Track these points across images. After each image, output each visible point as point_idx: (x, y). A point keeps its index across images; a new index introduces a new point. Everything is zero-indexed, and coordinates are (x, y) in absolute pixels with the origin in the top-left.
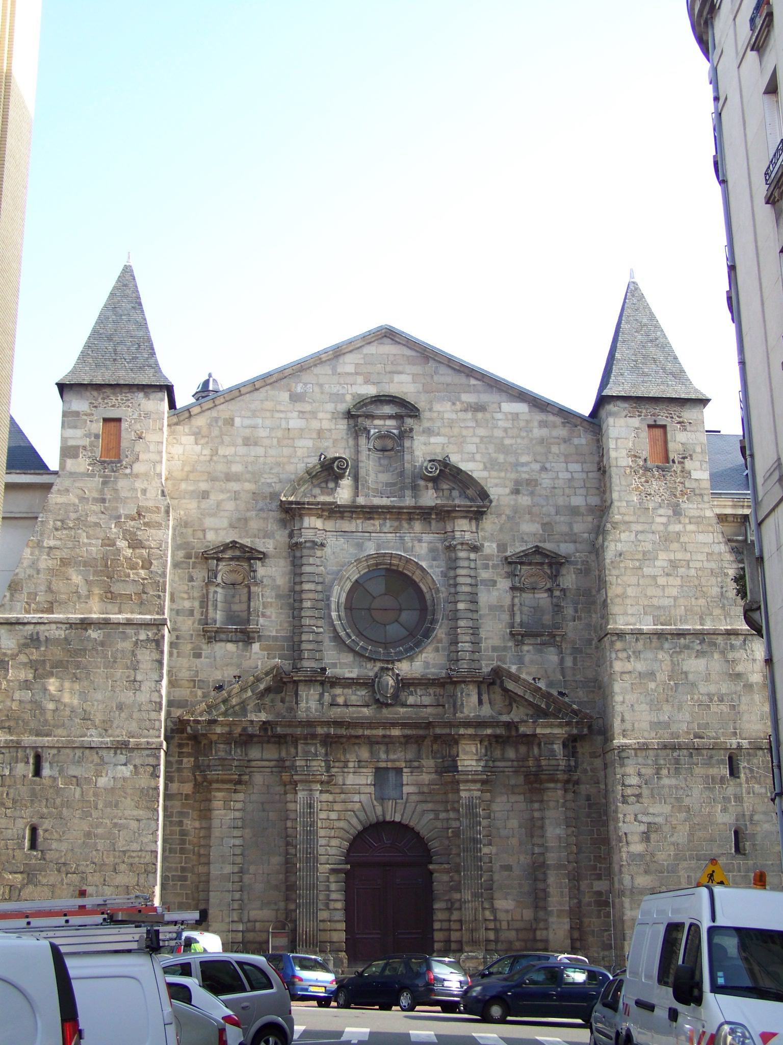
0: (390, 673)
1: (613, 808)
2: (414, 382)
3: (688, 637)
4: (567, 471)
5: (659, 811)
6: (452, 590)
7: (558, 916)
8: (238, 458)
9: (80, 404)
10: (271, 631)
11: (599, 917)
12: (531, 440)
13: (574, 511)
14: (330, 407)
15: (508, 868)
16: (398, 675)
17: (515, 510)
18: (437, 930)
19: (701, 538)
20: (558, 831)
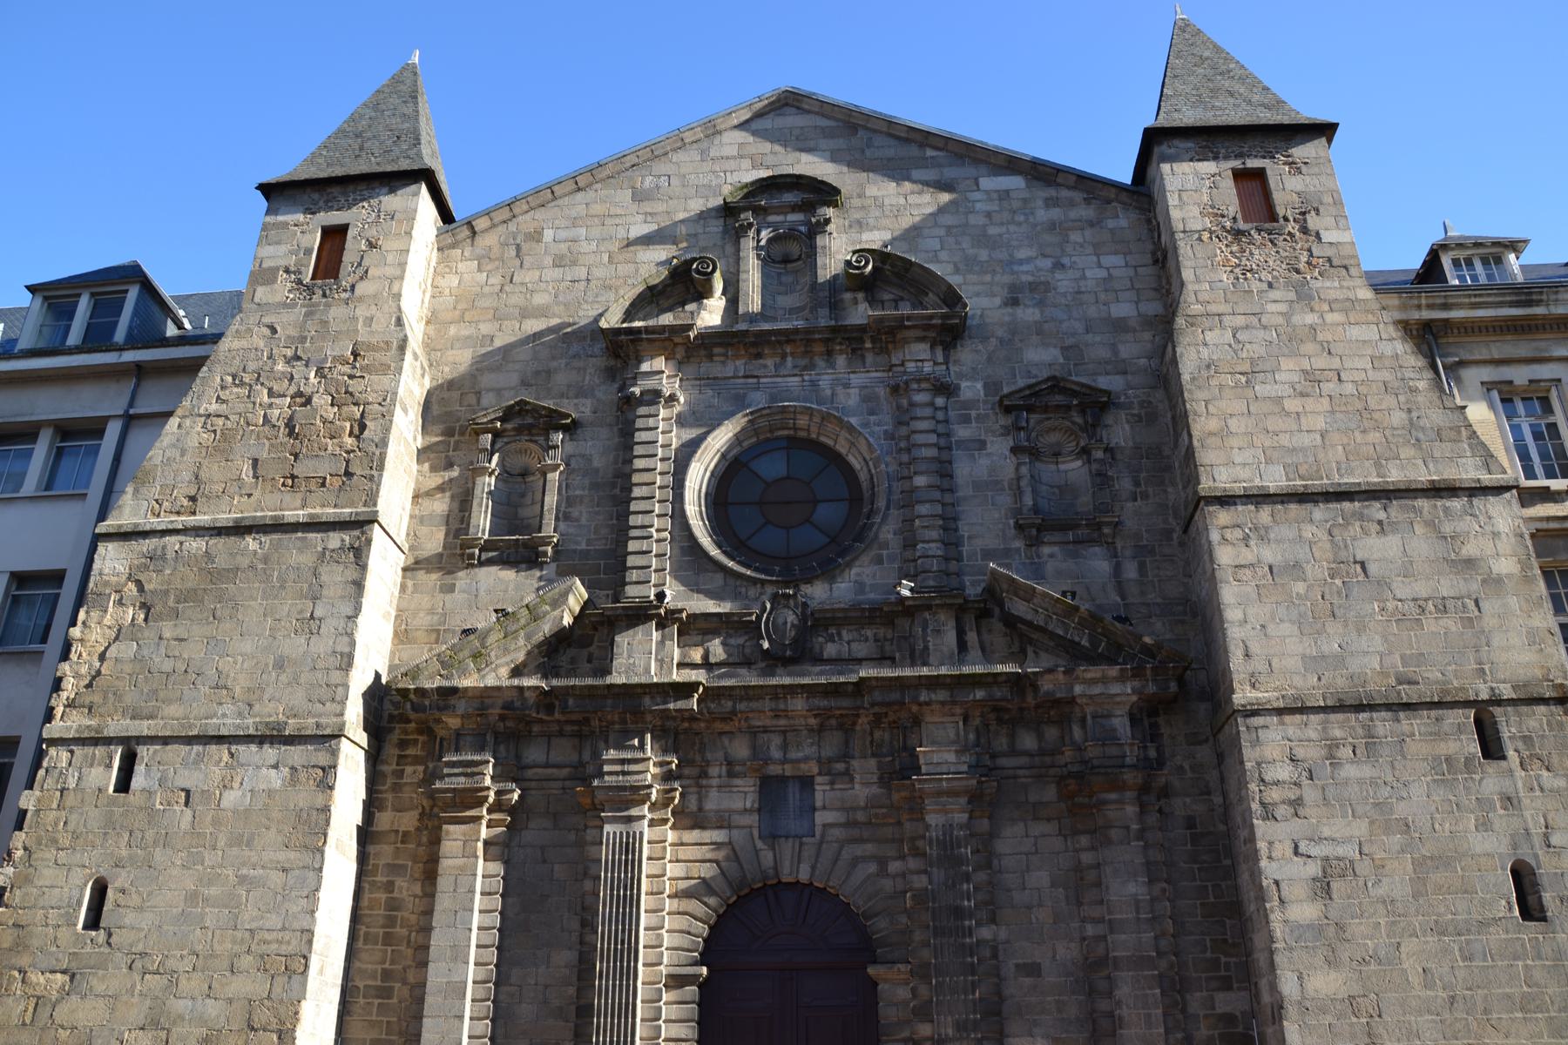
1: (1243, 834)
4: (1100, 266)
5: (1342, 833)
6: (905, 458)
10: (577, 543)
13: (1119, 326)
15: (1033, 970)
16: (805, 605)
19: (1355, 332)
20: (1132, 888)
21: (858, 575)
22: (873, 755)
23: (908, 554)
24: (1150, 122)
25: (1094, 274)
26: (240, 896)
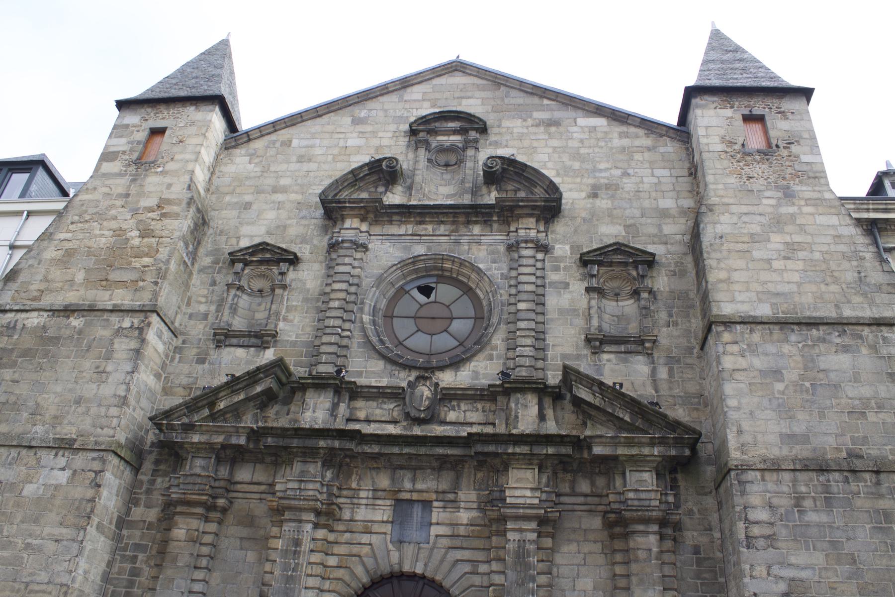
0: (428, 383)
2: (483, 104)
3: (821, 328)
4: (653, 176)
6: (513, 291)
9: (132, 118)
10: (290, 336)
12: (611, 148)
13: (664, 214)
14: (393, 127)
17: (593, 213)
19: (821, 220)
21: (475, 366)
22: (475, 489)
23: (511, 354)
24: (691, 83)
25: (649, 180)
26: (22, 558)
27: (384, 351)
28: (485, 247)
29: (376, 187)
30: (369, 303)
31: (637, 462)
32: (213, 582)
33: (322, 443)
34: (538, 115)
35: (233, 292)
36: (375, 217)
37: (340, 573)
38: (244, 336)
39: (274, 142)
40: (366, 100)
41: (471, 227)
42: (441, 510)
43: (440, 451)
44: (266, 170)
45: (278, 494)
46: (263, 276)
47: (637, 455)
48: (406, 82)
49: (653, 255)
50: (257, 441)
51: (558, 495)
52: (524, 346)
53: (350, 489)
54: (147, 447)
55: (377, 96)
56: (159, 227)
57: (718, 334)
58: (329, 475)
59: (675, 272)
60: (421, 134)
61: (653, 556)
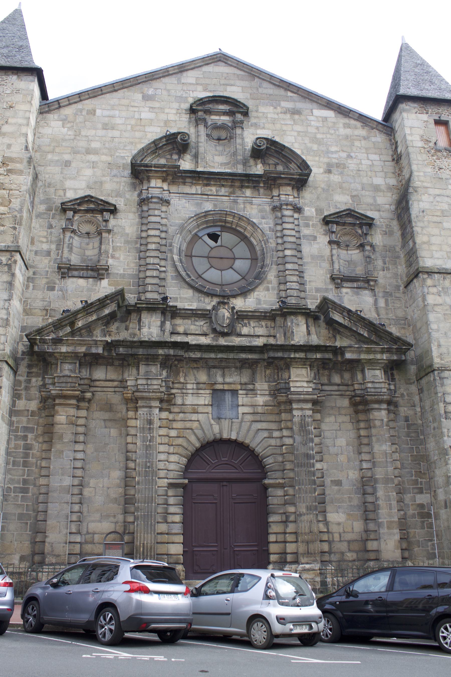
0: (226, 307)
2: (243, 92)
4: (368, 159)
7: (388, 528)
8: (97, 138)
10: (119, 270)
11: (423, 528)
12: (339, 136)
13: (376, 189)
15: (338, 483)
18: (273, 542)
21: (258, 295)
22: (266, 382)
27: (192, 283)
28: (256, 206)
29: (171, 155)
30: (176, 246)
31: (372, 363)
32: (89, 451)
33: (161, 352)
34: (283, 104)
35: (68, 234)
36: (172, 179)
37: (180, 441)
38: (83, 270)
39: (81, 110)
40: (151, 80)
41: (244, 190)
42: (245, 396)
43: (243, 356)
44: (78, 134)
45: (129, 388)
46: (89, 222)
47: (373, 359)
48: (182, 67)
49: (373, 219)
50: (110, 351)
51: (322, 385)
52: (292, 282)
53: (180, 383)
54: (19, 355)
55: (160, 78)
56: (7, 181)
57: (424, 280)
58: (164, 373)
59: (386, 232)
60: (200, 113)
61: (384, 424)
